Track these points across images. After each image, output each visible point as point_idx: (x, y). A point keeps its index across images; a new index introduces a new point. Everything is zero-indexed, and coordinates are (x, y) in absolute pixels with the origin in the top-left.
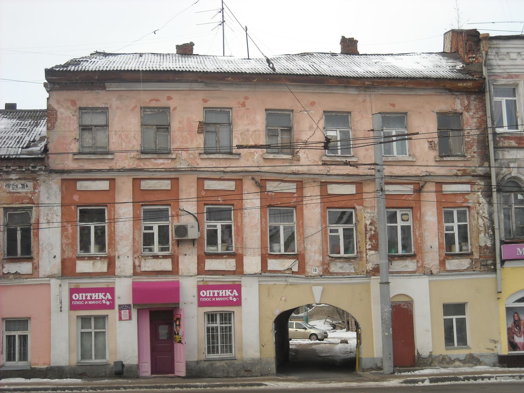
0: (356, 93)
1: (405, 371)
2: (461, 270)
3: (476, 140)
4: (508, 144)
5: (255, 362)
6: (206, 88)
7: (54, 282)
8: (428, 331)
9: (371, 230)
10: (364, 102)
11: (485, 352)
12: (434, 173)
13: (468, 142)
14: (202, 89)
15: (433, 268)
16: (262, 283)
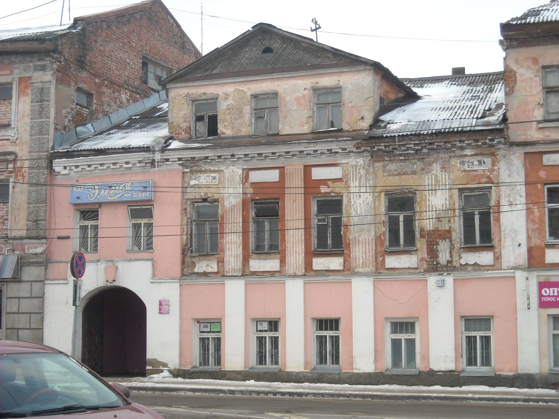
1: (79, 156)
7: (520, 275)
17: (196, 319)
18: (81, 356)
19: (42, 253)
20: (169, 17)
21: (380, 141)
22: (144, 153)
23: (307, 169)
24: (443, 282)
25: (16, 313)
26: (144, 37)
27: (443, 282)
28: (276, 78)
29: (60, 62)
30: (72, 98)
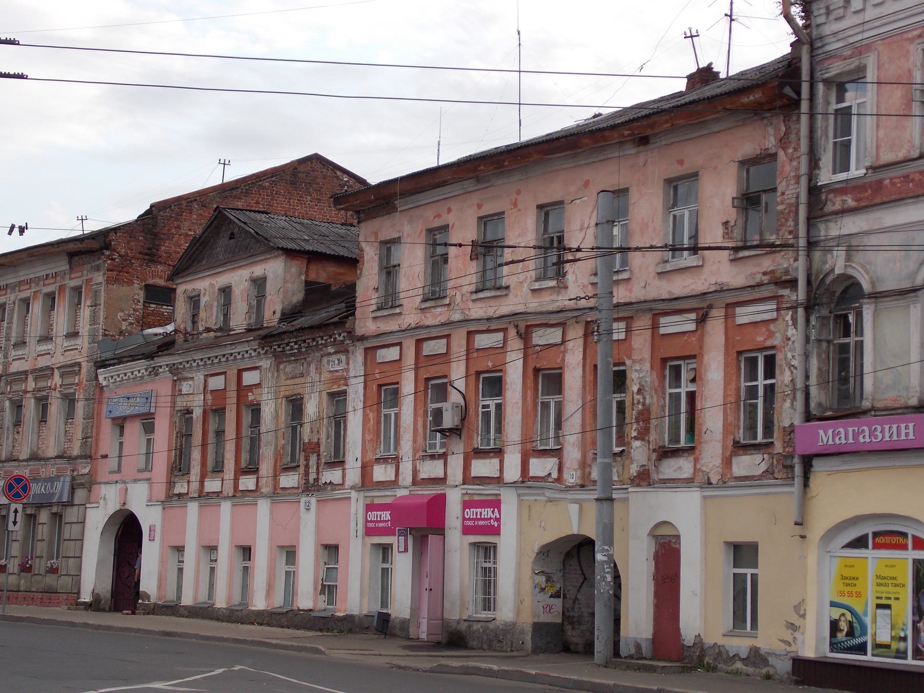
0: (633, 151)
2: (757, 476)
3: (794, 205)
4: (840, 205)
5: (509, 629)
6: (479, 187)
7: (354, 495)
8: (696, 595)
9: (639, 403)
10: (644, 165)
11: (780, 648)
12: (727, 283)
13: (782, 212)
14: (475, 188)
15: (713, 472)
16: (524, 498)
17: (175, 547)
18: (110, 588)
19: (88, 474)
20: (339, 173)
21: (272, 340)
22: (143, 361)
23: (240, 372)
24: (307, 504)
25: (68, 540)
26: (281, 207)
27: (307, 504)
28: (238, 267)
29: (113, 259)
30: (136, 297)
